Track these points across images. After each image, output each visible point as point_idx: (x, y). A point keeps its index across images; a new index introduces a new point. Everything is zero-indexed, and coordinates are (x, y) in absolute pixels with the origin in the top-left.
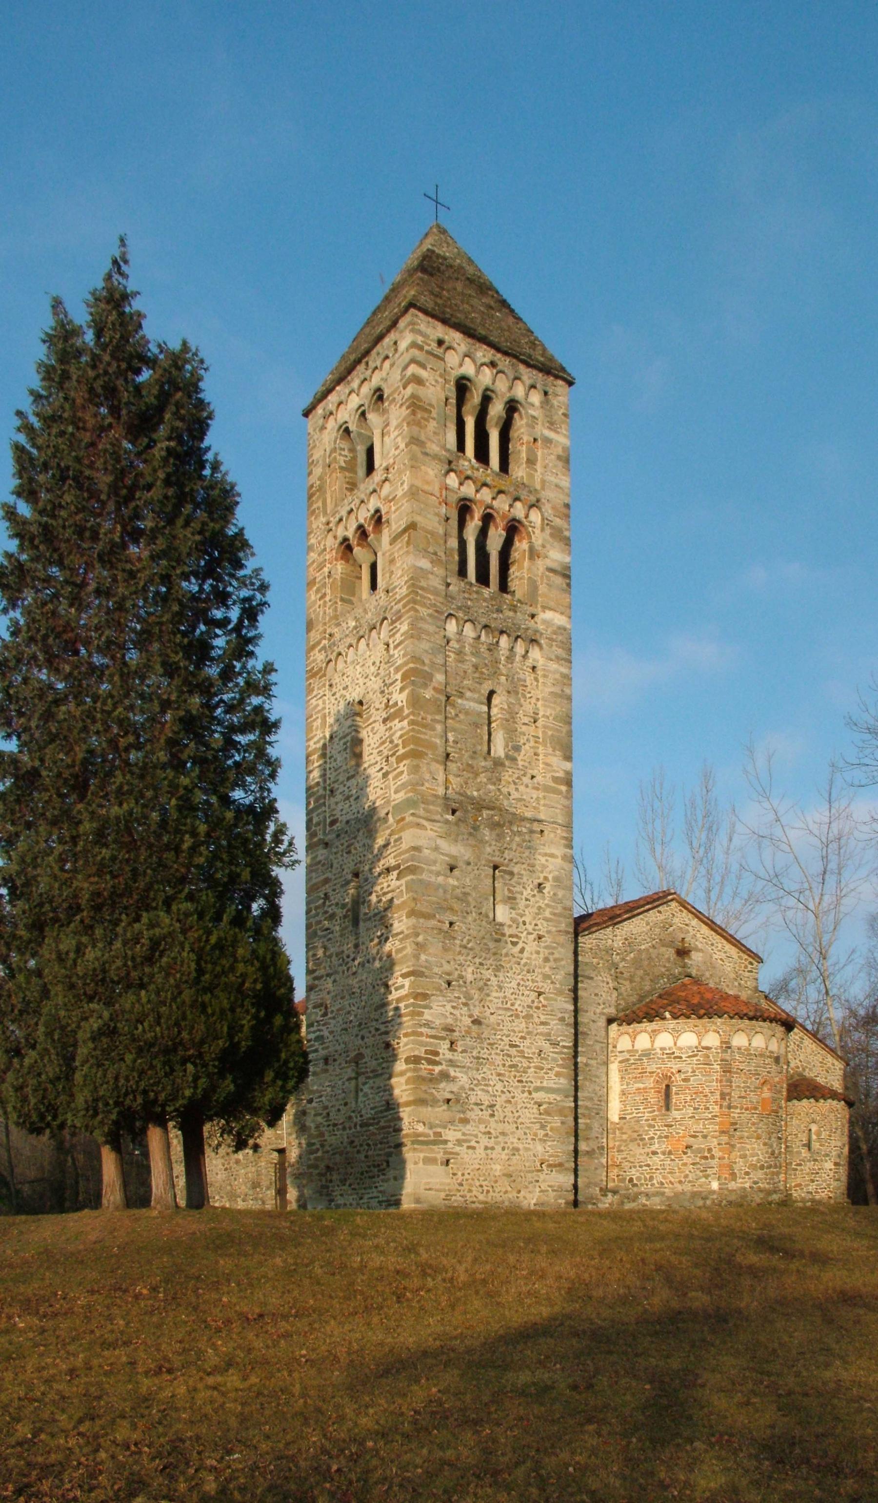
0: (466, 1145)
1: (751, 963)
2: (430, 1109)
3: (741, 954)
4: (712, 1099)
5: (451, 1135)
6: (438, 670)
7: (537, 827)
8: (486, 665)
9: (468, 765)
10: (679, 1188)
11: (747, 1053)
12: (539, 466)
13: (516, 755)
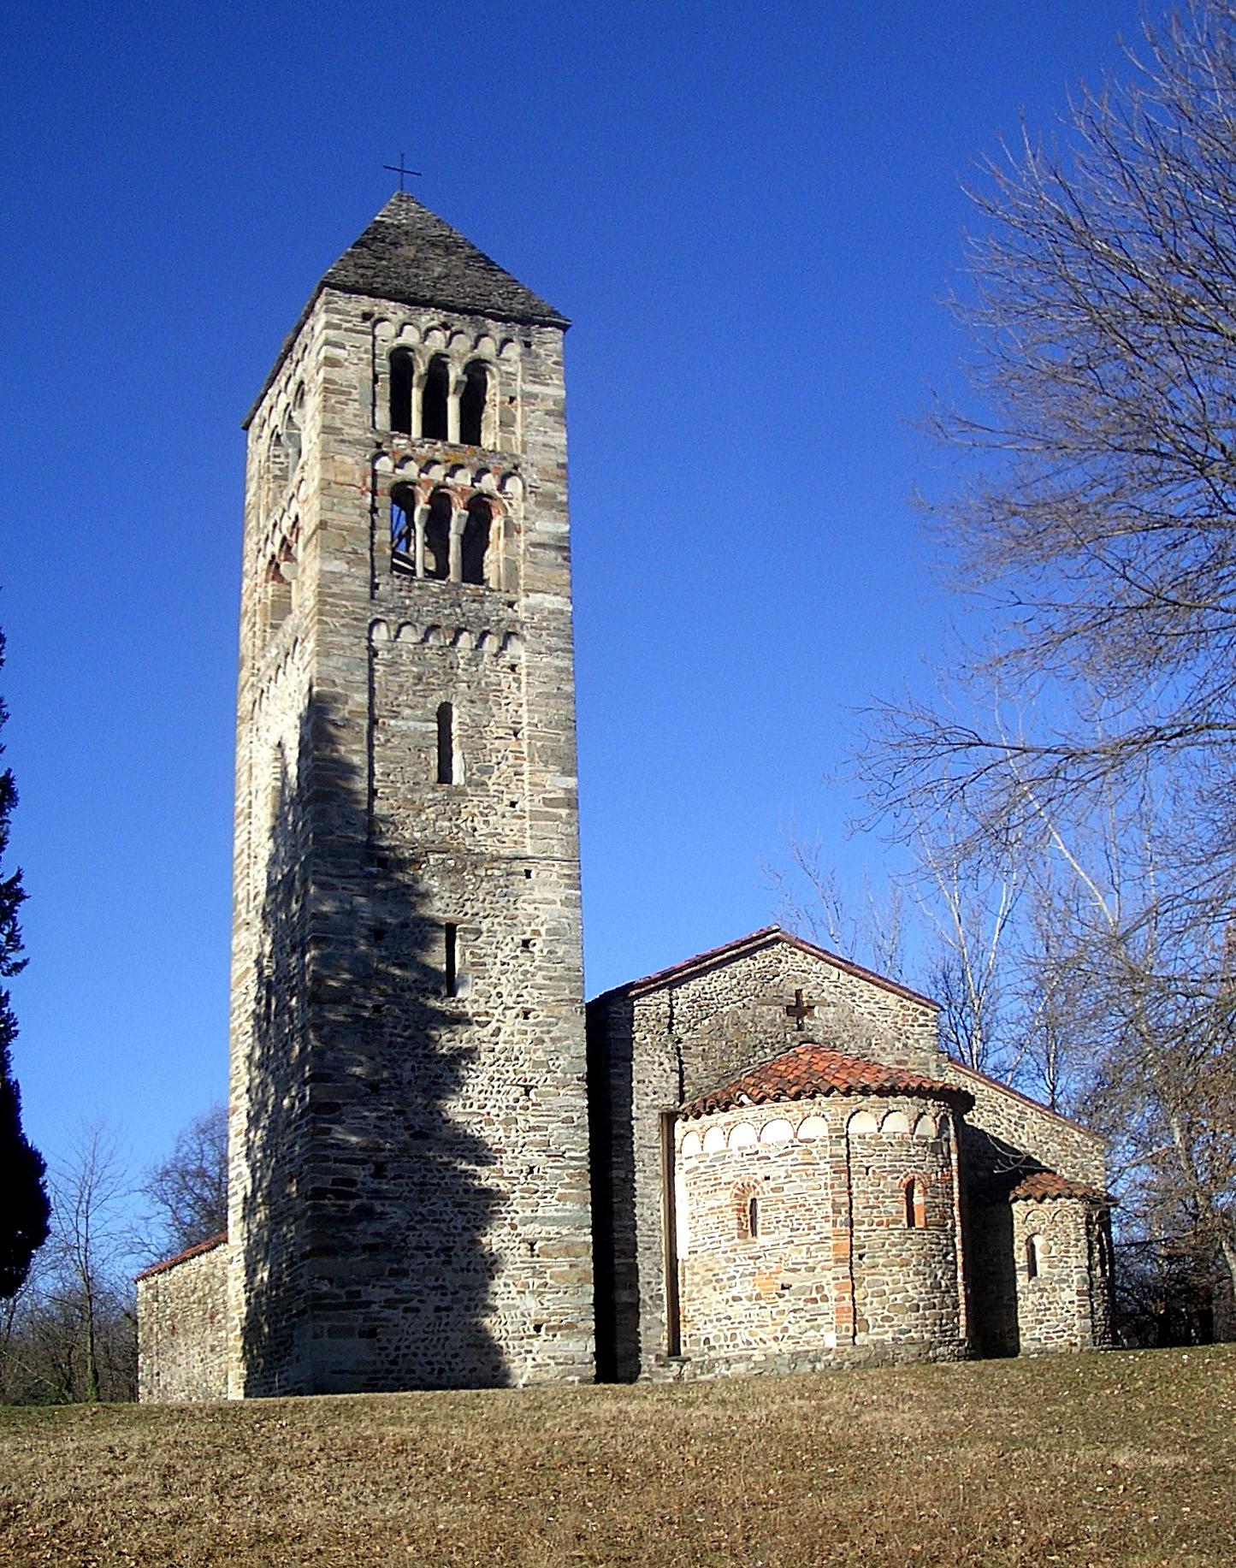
0: (402, 1306)
1: (924, 1014)
2: (340, 1259)
3: (906, 1002)
5: (376, 1293)
6: (357, 690)
7: (520, 867)
8: (435, 673)
9: (406, 799)
10: (774, 1348)
11: (877, 1143)
12: (518, 429)
13: (485, 778)
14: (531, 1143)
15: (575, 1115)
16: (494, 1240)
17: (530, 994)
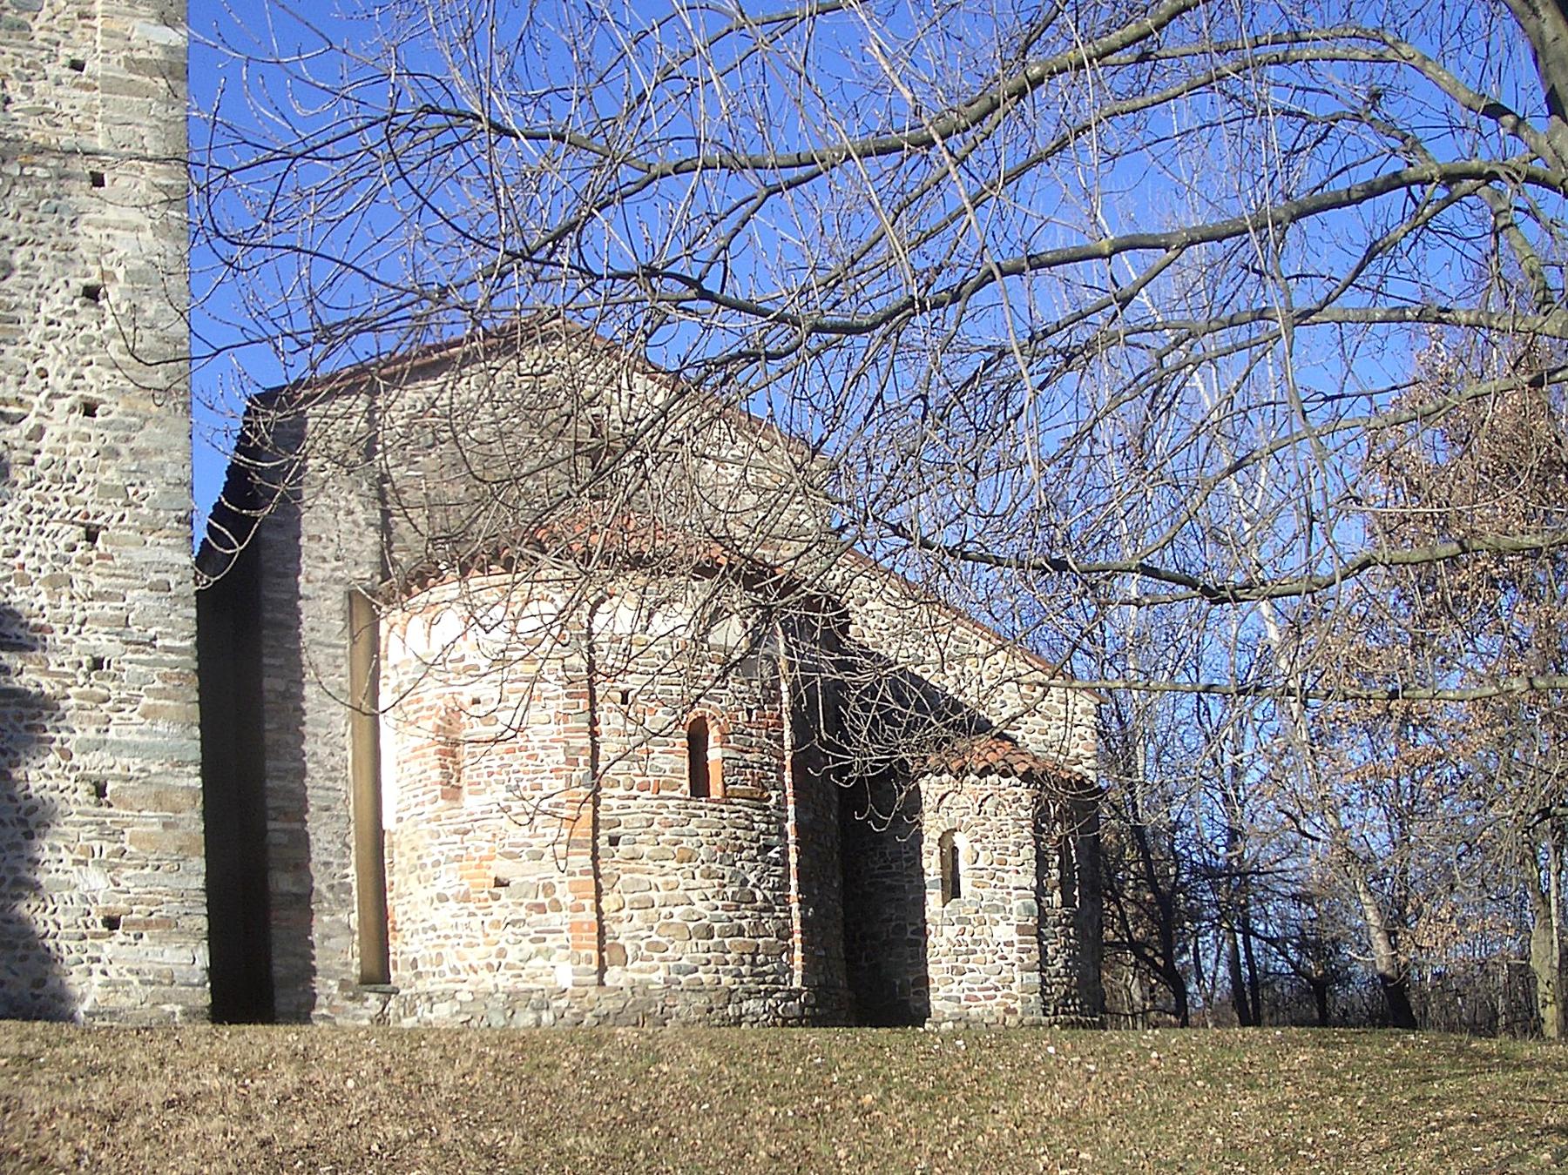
7: (79, 165)
10: (488, 981)
13: (26, 17)
14: (96, 619)
15: (172, 579)
16: (33, 774)
17: (97, 376)
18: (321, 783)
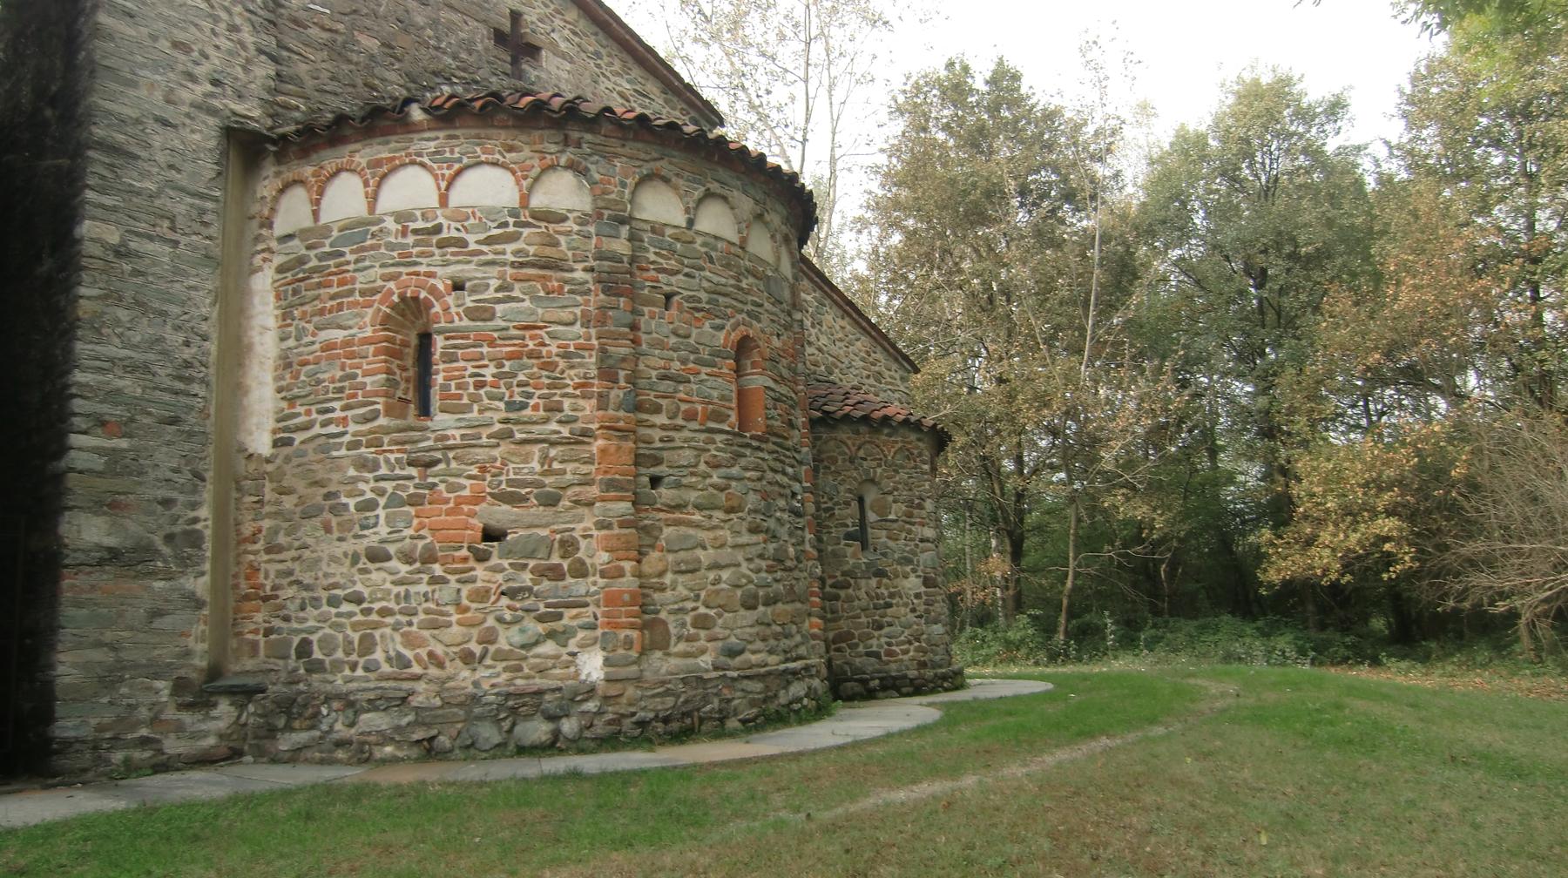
4: (572, 377)
10: (464, 677)
18: (168, 382)
